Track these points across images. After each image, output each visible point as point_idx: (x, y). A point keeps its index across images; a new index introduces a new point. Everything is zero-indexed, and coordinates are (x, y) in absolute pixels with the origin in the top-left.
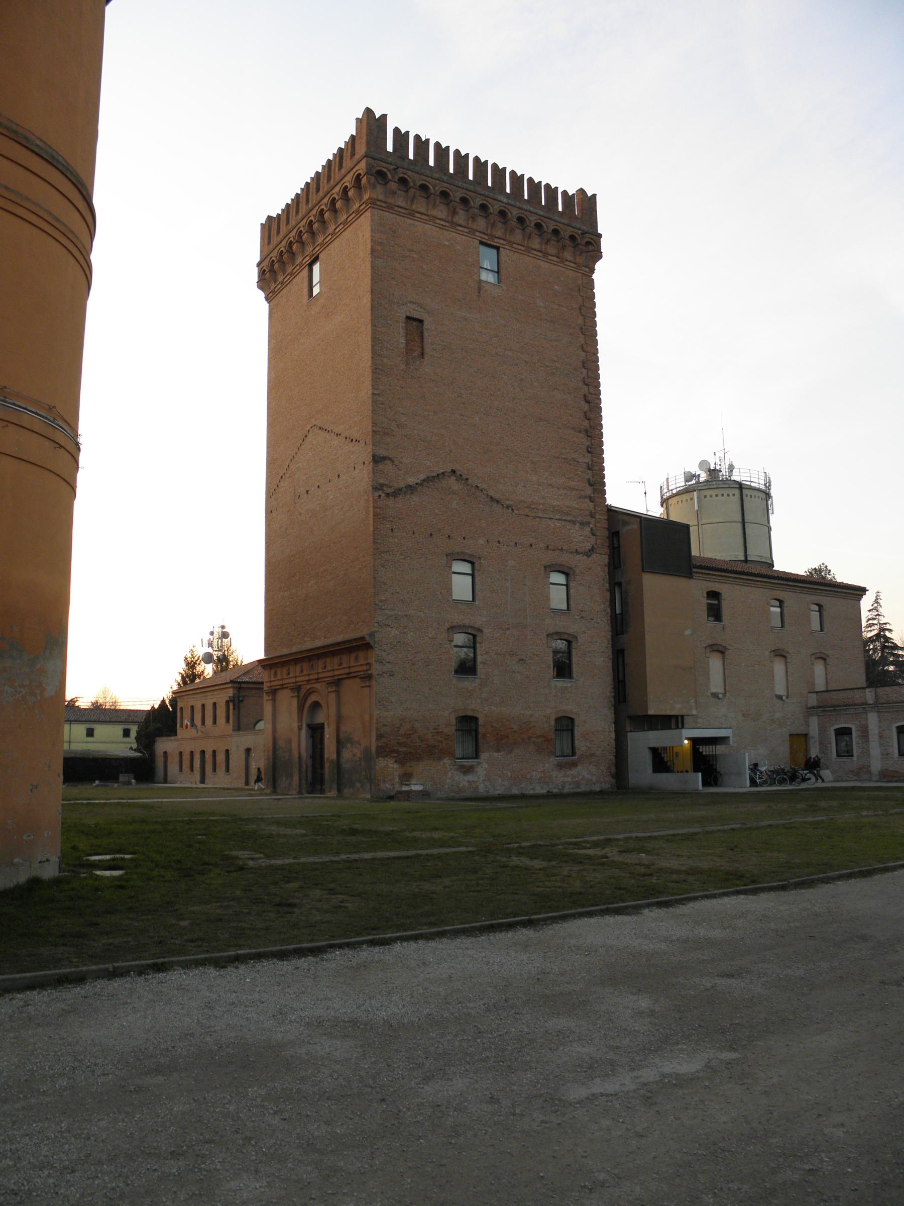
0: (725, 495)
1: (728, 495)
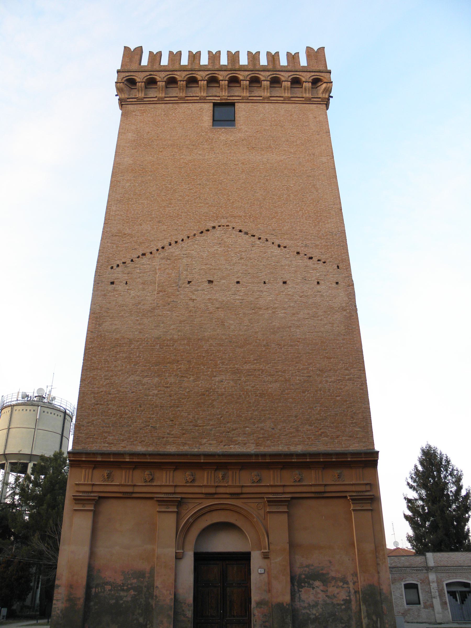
0: (56, 415)
1: (58, 415)
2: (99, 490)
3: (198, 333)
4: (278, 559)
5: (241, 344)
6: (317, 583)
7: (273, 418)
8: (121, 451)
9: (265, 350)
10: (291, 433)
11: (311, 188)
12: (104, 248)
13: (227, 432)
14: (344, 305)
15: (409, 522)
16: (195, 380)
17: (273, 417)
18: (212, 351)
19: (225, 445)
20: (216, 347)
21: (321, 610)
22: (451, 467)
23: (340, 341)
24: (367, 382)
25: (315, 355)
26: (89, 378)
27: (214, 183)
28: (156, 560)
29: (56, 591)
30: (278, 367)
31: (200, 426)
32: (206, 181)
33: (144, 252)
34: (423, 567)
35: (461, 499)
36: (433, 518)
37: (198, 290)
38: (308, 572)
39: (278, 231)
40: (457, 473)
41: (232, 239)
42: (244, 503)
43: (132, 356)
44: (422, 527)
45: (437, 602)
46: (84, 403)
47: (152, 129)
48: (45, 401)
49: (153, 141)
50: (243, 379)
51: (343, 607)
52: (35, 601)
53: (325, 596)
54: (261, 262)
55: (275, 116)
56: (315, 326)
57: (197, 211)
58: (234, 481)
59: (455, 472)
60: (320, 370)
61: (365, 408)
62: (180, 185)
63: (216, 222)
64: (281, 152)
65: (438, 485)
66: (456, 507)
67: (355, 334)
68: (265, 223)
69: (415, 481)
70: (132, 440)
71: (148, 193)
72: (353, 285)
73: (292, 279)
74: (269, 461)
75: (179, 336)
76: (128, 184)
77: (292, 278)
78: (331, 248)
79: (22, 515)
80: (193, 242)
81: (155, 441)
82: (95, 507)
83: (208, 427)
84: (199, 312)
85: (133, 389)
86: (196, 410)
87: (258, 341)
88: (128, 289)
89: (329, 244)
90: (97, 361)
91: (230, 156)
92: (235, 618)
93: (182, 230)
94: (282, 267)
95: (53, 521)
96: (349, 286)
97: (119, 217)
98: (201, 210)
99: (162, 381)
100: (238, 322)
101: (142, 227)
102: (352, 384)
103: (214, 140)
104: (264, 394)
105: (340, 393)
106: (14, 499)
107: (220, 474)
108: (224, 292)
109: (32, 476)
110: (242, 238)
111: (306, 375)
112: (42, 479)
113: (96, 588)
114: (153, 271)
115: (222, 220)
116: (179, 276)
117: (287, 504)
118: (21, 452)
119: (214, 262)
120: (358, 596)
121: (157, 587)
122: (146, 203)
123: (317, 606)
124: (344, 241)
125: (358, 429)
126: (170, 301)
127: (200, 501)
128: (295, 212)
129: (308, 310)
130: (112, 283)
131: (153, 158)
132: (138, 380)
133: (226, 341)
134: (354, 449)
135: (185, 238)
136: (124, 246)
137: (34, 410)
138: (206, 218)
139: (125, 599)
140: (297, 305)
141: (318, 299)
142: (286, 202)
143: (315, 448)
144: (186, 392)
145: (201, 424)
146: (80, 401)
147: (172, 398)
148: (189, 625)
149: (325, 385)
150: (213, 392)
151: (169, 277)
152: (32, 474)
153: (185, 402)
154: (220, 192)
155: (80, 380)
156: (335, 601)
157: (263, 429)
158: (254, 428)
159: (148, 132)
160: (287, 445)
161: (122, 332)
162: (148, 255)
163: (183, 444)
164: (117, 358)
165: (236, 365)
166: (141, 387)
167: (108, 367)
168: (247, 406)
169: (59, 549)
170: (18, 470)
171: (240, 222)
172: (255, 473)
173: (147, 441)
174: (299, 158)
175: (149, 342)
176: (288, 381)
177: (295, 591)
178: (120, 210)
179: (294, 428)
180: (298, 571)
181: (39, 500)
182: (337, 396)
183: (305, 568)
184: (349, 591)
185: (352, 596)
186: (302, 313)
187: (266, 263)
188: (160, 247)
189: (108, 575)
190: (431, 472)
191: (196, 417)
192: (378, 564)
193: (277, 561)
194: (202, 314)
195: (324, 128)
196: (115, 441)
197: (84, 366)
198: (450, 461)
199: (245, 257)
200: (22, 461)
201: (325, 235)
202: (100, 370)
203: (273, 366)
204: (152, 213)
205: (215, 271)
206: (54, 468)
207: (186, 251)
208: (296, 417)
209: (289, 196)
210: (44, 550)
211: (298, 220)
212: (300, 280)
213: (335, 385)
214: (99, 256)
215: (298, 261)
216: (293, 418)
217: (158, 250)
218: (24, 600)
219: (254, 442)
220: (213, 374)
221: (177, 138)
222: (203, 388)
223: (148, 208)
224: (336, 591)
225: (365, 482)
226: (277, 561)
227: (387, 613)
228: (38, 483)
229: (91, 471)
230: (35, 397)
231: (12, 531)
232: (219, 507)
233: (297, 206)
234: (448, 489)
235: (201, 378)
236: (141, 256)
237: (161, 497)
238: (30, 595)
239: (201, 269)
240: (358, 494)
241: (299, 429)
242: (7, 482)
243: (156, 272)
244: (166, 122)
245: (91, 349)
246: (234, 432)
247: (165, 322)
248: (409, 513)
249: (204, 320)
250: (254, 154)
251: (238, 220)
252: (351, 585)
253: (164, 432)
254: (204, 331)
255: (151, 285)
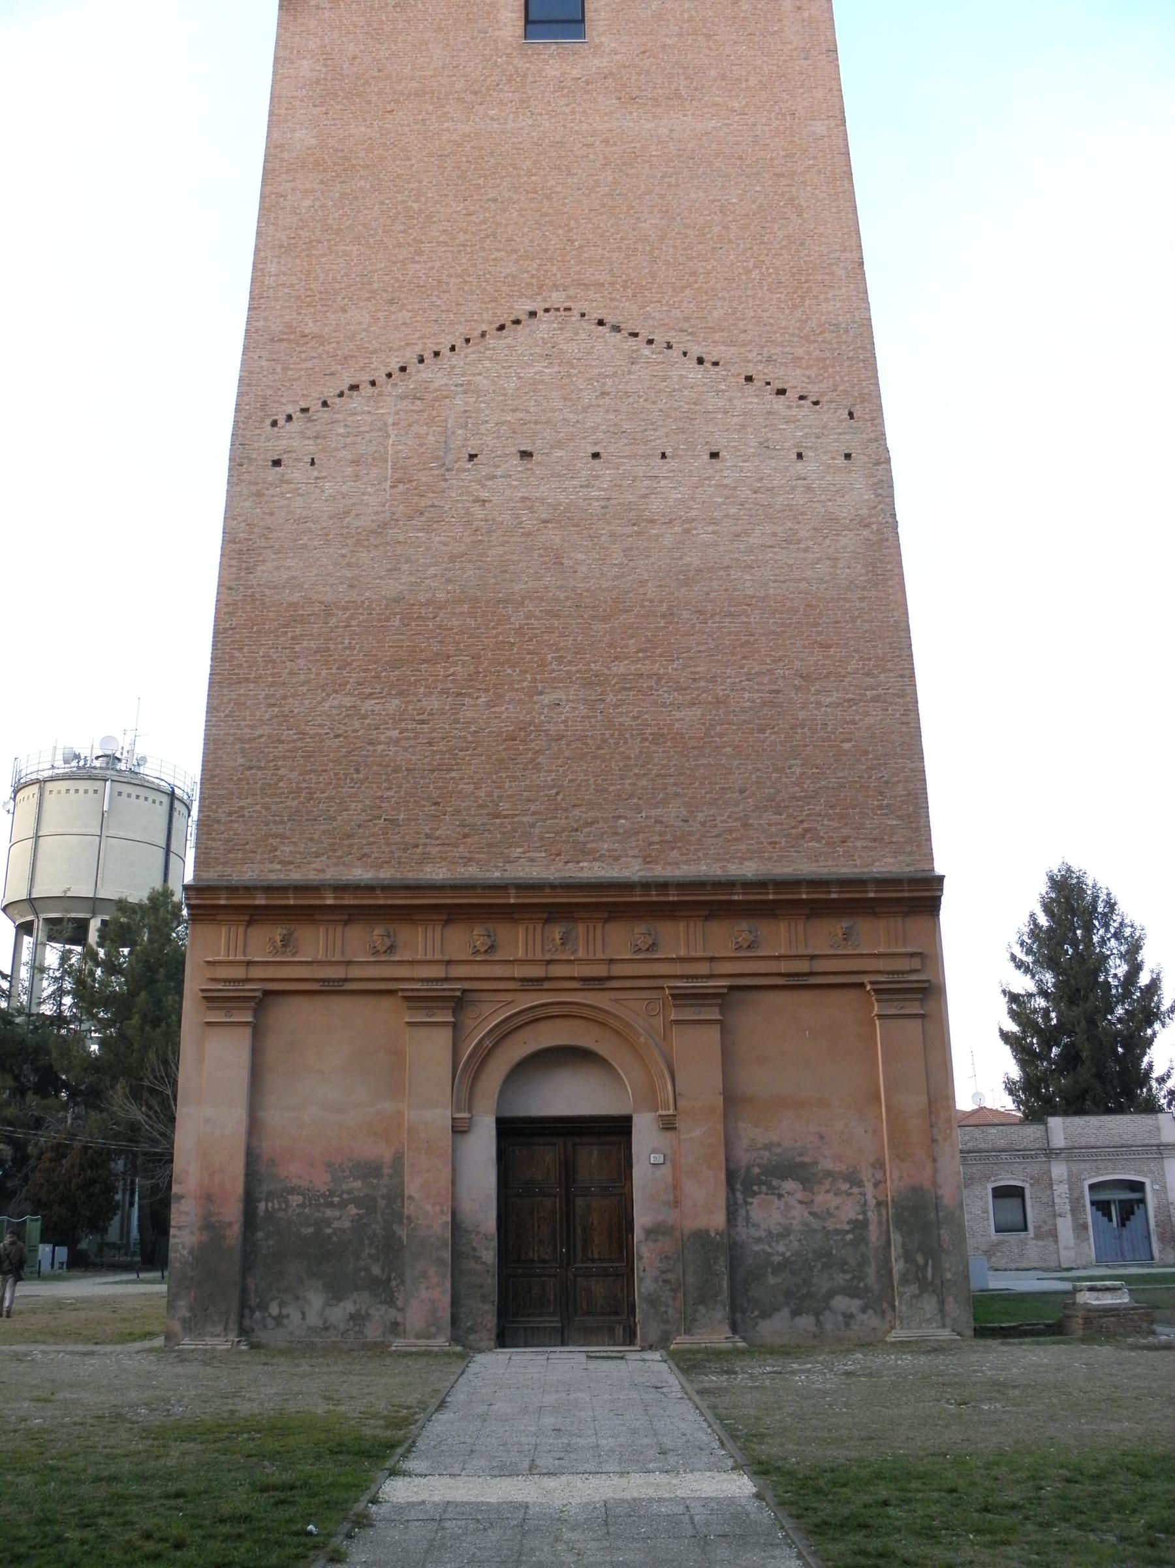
0: (150, 800)
1: (154, 802)
2: (265, 977)
3: (496, 584)
4: (699, 1132)
5: (605, 611)
6: (789, 1185)
7: (686, 795)
8: (314, 880)
9: (664, 627)
10: (730, 832)
11: (785, 206)
12: (251, 373)
13: (571, 831)
14: (864, 512)
15: (1011, 1047)
16: (491, 704)
17: (685, 791)
18: (533, 629)
19: (566, 863)
20: (541, 618)
21: (796, 1244)
22: (1119, 919)
23: (853, 604)
24: (920, 705)
25: (790, 638)
26: (229, 703)
27: (530, 196)
28: (405, 1136)
29: (174, 1207)
30: (698, 669)
31: (506, 817)
32: (509, 191)
33: (354, 381)
34: (1038, 1149)
35: (1138, 994)
36: (1068, 1037)
37: (495, 477)
38: (768, 1159)
39: (698, 321)
40: (1133, 932)
41: (578, 344)
42: (616, 1000)
43: (332, 647)
44: (1042, 1060)
45: (1065, 1227)
46: (218, 766)
47: (362, 47)
48: (122, 766)
49: (366, 83)
50: (611, 698)
51: (850, 1237)
52: (129, 1232)
53: (806, 1214)
54: (654, 403)
55: (692, 6)
56: (790, 566)
57: (489, 273)
58: (591, 949)
59: (1127, 931)
60: (801, 676)
61: (912, 770)
62: (444, 203)
63: (539, 298)
64: (706, 110)
65: (1084, 960)
66: (1125, 1013)
67: (892, 587)
68: (664, 302)
69: (1029, 952)
70: (339, 854)
71: (360, 224)
72: (888, 461)
73: (734, 447)
74: (676, 899)
75: (448, 593)
76: (307, 203)
77: (733, 444)
78: (833, 366)
79: (83, 1041)
80: (480, 352)
81: (396, 855)
82: (255, 1015)
83: (525, 819)
84: (499, 533)
85: (338, 729)
86: (494, 776)
87: (647, 603)
88: (317, 478)
89: (828, 354)
90: (247, 661)
91: (573, 121)
92: (595, 1265)
93: (451, 323)
94: (710, 416)
95: (157, 1053)
96: (878, 463)
97: (286, 290)
98: (499, 269)
99: (410, 708)
100: (597, 556)
101: (348, 315)
102: (883, 710)
103: (530, 79)
104: (662, 735)
105: (852, 733)
106: (61, 1004)
107: (556, 932)
108: (559, 481)
109: (100, 949)
110: (606, 342)
111: (767, 688)
112: (124, 956)
113: (267, 1201)
114: (380, 429)
115: (555, 295)
116: (445, 442)
117: (719, 1001)
118: (69, 894)
119: (533, 403)
120: (884, 1212)
121: (411, 1198)
122: (355, 253)
123: (789, 1236)
124: (869, 347)
125: (895, 823)
126: (424, 505)
127: (508, 997)
128: (741, 270)
129: (774, 524)
130: (277, 463)
131: (369, 130)
132: (349, 705)
133: (568, 603)
134: (883, 870)
135: (459, 343)
136: (304, 365)
137: (96, 791)
138: (512, 291)
139: (336, 1225)
140: (746, 512)
141: (800, 498)
142: (719, 246)
143: (789, 866)
144: (469, 732)
145: (507, 810)
146: (207, 761)
147: (435, 748)
148: (489, 1280)
149: (814, 712)
150: (537, 731)
151: (421, 445)
152: (100, 945)
153: (468, 758)
154: (547, 219)
155: (205, 709)
156: (830, 1225)
157: (662, 822)
158: (640, 819)
159: (354, 58)
160: (719, 860)
161: (306, 586)
162: (366, 390)
163: (466, 860)
164: (295, 652)
165: (592, 665)
166: (357, 724)
167: (273, 675)
168: (621, 764)
169: (175, 1118)
170: (66, 936)
171: (599, 299)
172: (640, 928)
173: (377, 855)
174: (754, 125)
175: (374, 609)
176: (722, 703)
177: (736, 1203)
178: (289, 272)
179: (739, 819)
180: (744, 1157)
181: (121, 1005)
182: (842, 742)
183: (762, 1152)
184: (862, 1202)
185: (870, 1214)
186: (757, 533)
187: (668, 406)
188: (394, 367)
189: (293, 1172)
190: (1070, 930)
191: (496, 794)
192: (934, 1141)
193: (692, 1135)
194: (505, 538)
195: (823, 38)
196: (298, 856)
197: (215, 674)
198: (1115, 904)
199: (614, 390)
200: (73, 915)
201: (818, 332)
202: (253, 682)
203: (685, 666)
204: (371, 278)
205: (538, 427)
206: (153, 929)
207: (462, 375)
208: (742, 791)
209: (726, 228)
210: (140, 1122)
211: (749, 293)
212: (754, 447)
213: (839, 713)
214: (240, 395)
215: (749, 400)
216: (735, 795)
217: (389, 375)
218: (105, 1230)
219: (640, 854)
220: (537, 687)
221: (431, 73)
222: (511, 722)
223: (361, 267)
224: (833, 1201)
225: (910, 950)
226: (692, 1135)
227: (951, 1248)
228: (115, 965)
229: (241, 930)
230: (97, 758)
231: (61, 1079)
232: (555, 1011)
233: (748, 254)
234: (1107, 971)
235: (507, 698)
236: (346, 392)
237: (413, 990)
238: (116, 1220)
239: (502, 423)
240: (891, 978)
241: (750, 821)
242: (40, 965)
243: (386, 432)
244: (400, 26)
245: (230, 632)
246: (589, 829)
247: (413, 558)
248: (1012, 1027)
249: (512, 553)
250: (635, 114)
251: (595, 293)
252: (869, 1188)
253: (418, 833)
254: (512, 581)
255: (375, 466)
